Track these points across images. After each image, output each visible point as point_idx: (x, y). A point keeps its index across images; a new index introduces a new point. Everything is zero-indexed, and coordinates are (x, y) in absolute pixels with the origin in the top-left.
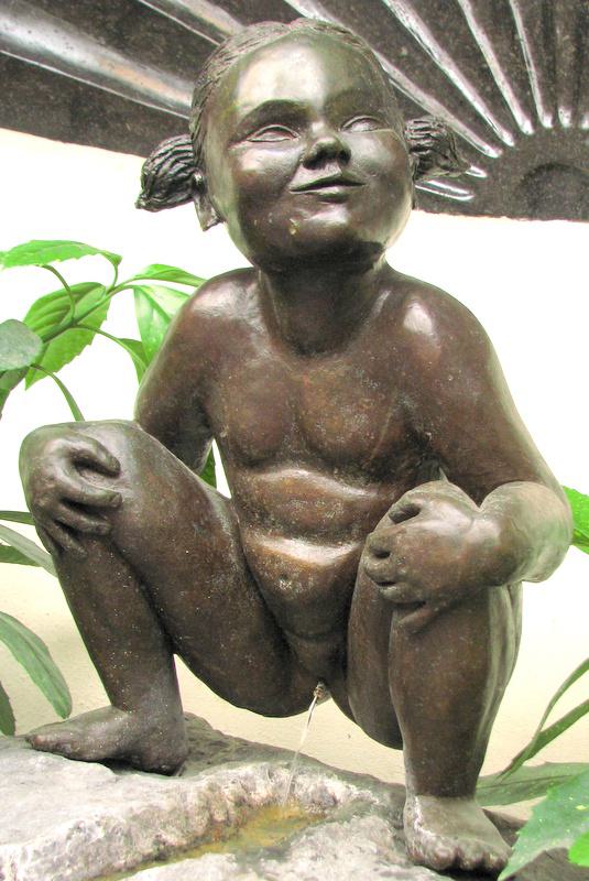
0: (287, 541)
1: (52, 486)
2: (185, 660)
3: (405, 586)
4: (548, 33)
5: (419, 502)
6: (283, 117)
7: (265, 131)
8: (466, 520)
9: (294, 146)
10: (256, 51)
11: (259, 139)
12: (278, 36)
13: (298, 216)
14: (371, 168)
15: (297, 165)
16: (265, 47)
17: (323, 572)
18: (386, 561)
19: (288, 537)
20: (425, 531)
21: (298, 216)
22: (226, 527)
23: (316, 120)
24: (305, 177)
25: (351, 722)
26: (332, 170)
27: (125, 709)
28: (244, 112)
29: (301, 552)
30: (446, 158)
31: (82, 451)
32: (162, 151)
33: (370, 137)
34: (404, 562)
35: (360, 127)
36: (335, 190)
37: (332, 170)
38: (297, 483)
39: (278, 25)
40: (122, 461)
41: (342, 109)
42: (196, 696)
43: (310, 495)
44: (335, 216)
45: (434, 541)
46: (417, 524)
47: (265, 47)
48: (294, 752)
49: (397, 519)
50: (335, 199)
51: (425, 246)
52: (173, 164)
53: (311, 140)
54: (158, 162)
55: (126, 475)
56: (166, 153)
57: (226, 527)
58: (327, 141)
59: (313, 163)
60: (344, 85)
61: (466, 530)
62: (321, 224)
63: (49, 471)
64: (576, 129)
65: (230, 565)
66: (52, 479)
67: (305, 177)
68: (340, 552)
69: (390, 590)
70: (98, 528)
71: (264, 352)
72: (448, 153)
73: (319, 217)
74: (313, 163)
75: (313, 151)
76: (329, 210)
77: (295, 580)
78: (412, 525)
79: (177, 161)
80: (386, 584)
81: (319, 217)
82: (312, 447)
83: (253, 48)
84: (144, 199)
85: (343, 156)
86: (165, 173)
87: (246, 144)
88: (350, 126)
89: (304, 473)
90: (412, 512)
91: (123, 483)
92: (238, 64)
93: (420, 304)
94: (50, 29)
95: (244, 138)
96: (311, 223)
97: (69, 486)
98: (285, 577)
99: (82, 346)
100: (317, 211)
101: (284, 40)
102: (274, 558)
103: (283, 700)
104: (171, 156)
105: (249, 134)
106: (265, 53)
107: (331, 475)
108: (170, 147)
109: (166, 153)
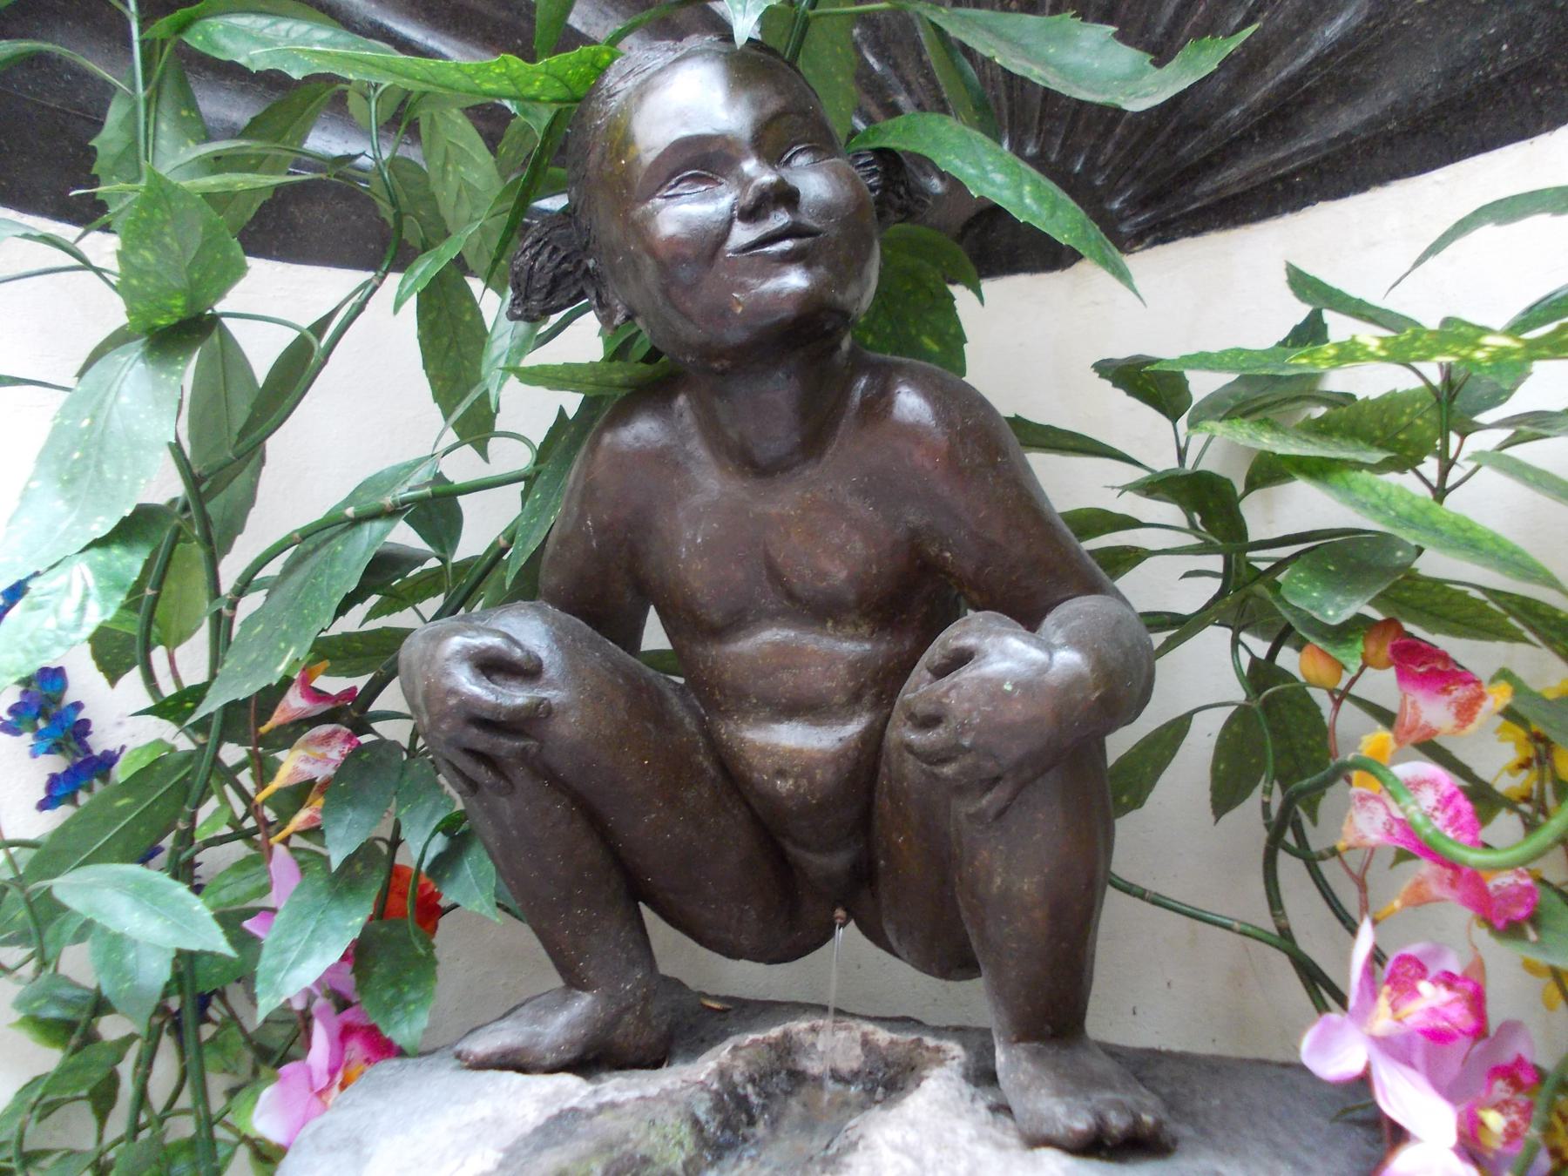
0: (776, 726)
1: (452, 701)
2: (1255, 634)
3: (969, 760)
5: (970, 641)
6: (701, 160)
8: (1037, 655)
9: (723, 196)
10: (646, 81)
12: (672, 56)
13: (742, 287)
14: (827, 210)
15: (730, 222)
16: (661, 70)
17: (836, 758)
18: (940, 730)
19: (779, 721)
20: (989, 680)
21: (742, 287)
22: (689, 722)
24: (742, 234)
25: (896, 960)
26: (780, 219)
27: (585, 988)
28: (649, 158)
29: (792, 736)
30: (900, 197)
31: (490, 648)
33: (815, 170)
34: (963, 728)
35: (801, 160)
36: (787, 245)
37: (780, 219)
38: (780, 648)
39: (670, 43)
40: (543, 654)
41: (771, 141)
42: (674, 952)
44: (795, 280)
45: (993, 690)
46: (975, 673)
47: (661, 70)
49: (941, 672)
50: (788, 258)
53: (745, 182)
55: (551, 672)
57: (689, 722)
58: (768, 178)
59: (751, 214)
60: (773, 105)
61: (1044, 669)
62: (776, 293)
63: (448, 683)
65: (703, 771)
66: (453, 692)
67: (742, 234)
68: (853, 728)
69: (948, 770)
70: (524, 749)
72: (902, 190)
73: (771, 285)
74: (751, 214)
75: (750, 197)
76: (784, 274)
77: (797, 778)
78: (967, 674)
80: (944, 761)
81: (771, 285)
82: (790, 595)
83: (644, 76)
85: (785, 196)
87: (658, 201)
88: (788, 161)
90: (962, 658)
91: (550, 684)
92: (627, 99)
93: (909, 385)
95: (652, 196)
96: (760, 295)
97: (478, 698)
98: (781, 773)
100: (766, 276)
101: (677, 60)
102: (764, 751)
103: (793, 938)
105: (659, 189)
106: (660, 78)
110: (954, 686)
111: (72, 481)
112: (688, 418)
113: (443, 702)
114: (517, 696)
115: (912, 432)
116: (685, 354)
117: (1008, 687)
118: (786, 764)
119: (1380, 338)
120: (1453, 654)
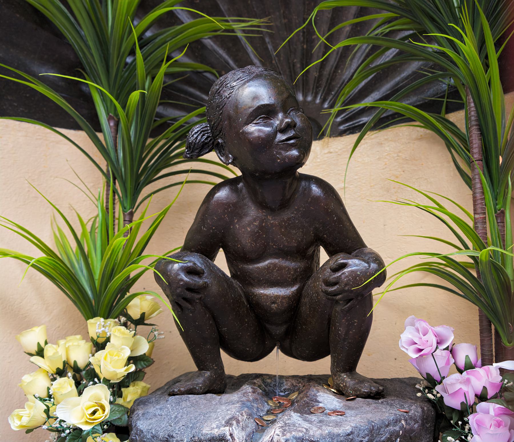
3: (345, 294)
4: (189, 100)
6: (265, 112)
7: (260, 119)
11: (258, 122)
17: (289, 297)
21: (280, 154)
23: (280, 112)
24: (280, 137)
26: (291, 133)
32: (196, 131)
36: (292, 141)
37: (291, 133)
38: (275, 265)
43: (281, 268)
44: (295, 152)
48: (275, 376)
50: (292, 146)
51: (326, 160)
52: (202, 137)
54: (195, 136)
56: (198, 132)
59: (283, 131)
64: (305, 101)
66: (182, 280)
67: (280, 137)
68: (294, 289)
71: (252, 212)
79: (203, 135)
80: (335, 295)
84: (189, 154)
86: (199, 142)
88: (289, 113)
89: (276, 261)
94: (44, 87)
98: (274, 303)
99: (480, 313)
100: (288, 151)
104: (200, 133)
105: (253, 121)
107: (287, 260)
108: (198, 129)
109: (198, 132)
110: (343, 273)
111: (172, 228)
112: (244, 191)
113: (178, 283)
114: (199, 281)
115: (316, 199)
116: (256, 173)
117: (359, 273)
118: (275, 299)
119: (497, 421)
120: (138, 241)
